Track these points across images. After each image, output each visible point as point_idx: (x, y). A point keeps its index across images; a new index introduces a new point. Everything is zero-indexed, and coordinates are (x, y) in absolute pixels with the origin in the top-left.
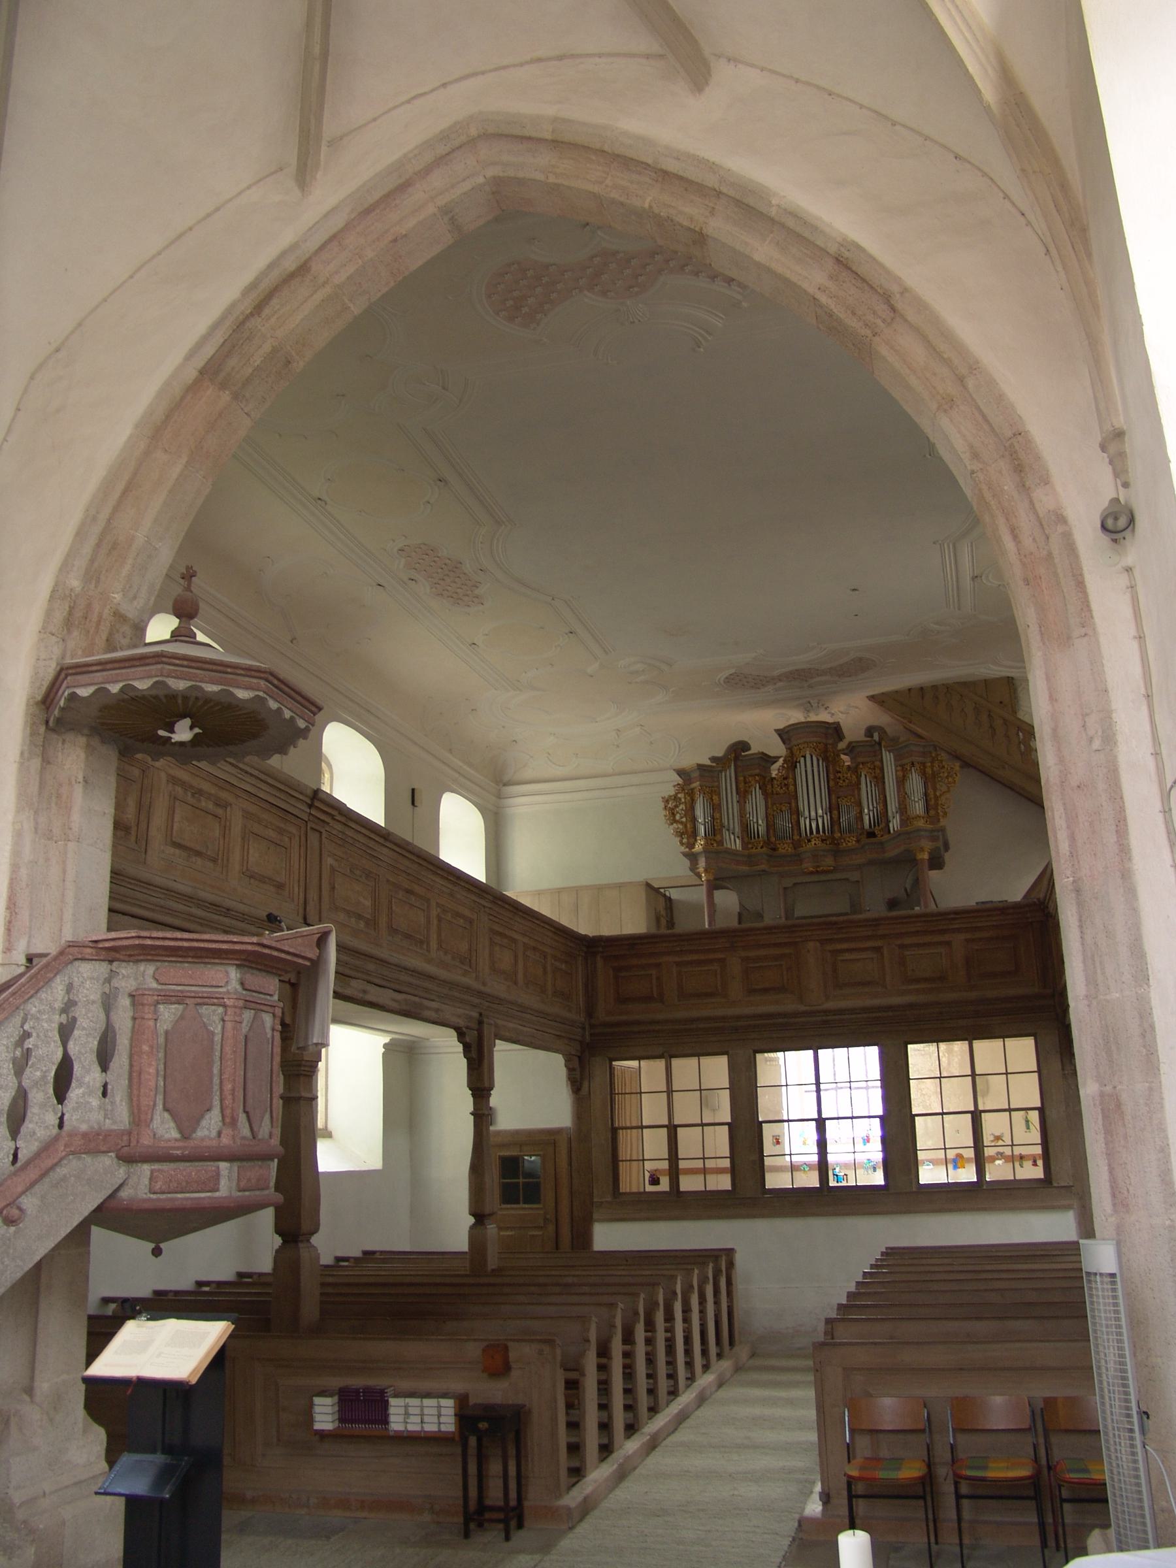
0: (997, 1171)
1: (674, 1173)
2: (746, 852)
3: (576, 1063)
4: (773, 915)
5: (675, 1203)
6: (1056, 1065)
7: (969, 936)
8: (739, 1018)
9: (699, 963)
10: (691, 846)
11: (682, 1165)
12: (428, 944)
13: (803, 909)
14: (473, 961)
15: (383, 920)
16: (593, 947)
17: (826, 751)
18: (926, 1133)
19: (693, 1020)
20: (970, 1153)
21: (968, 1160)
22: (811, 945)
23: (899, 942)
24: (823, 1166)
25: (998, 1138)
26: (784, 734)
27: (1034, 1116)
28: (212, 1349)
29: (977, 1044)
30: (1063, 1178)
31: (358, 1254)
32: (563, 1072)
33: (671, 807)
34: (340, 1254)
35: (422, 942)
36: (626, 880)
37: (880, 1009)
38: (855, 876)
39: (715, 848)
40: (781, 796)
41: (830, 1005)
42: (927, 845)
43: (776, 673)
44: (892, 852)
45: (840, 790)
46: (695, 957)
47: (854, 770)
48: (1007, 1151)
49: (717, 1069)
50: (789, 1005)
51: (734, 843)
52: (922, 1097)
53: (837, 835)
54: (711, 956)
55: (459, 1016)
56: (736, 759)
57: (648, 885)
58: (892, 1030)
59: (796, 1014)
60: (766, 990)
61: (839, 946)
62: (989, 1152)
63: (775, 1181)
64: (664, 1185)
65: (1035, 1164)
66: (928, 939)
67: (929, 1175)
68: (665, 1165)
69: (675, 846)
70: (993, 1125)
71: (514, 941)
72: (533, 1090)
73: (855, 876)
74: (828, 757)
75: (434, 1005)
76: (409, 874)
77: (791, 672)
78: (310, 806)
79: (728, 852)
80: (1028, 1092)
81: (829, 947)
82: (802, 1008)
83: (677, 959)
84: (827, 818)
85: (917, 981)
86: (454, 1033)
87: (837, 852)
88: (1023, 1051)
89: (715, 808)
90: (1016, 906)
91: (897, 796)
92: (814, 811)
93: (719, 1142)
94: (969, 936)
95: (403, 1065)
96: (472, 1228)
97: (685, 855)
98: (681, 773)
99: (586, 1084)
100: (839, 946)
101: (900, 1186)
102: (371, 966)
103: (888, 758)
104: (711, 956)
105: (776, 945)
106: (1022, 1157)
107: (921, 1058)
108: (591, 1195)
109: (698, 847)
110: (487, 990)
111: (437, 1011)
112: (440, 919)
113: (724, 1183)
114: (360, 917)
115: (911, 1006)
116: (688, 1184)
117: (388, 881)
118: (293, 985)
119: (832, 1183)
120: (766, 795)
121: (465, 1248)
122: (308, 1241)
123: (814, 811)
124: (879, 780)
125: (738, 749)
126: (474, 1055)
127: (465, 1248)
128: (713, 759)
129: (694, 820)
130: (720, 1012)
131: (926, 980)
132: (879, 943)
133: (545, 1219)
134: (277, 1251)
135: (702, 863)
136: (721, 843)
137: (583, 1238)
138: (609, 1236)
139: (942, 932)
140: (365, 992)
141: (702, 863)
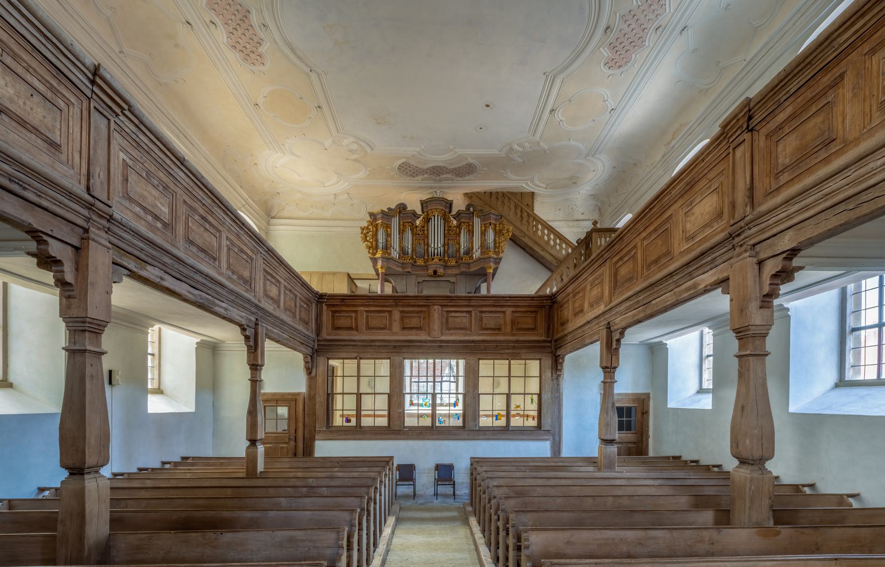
0: (516, 422)
1: (359, 416)
2: (401, 261)
3: (309, 359)
4: (412, 291)
5: (358, 432)
6: (548, 374)
7: (514, 309)
8: (398, 341)
9: (379, 312)
10: (374, 254)
11: (363, 413)
12: (220, 262)
13: (426, 292)
14: (253, 285)
15: (180, 230)
16: (321, 298)
17: (445, 215)
18: (485, 403)
19: (373, 341)
20: (504, 413)
21: (503, 416)
22: (436, 307)
23: (480, 309)
24: (433, 416)
25: (518, 407)
26: (423, 204)
27: (535, 398)
28: (767, 85)
29: (512, 361)
30: (546, 425)
31: (178, 460)
32: (302, 364)
33: (365, 232)
34: (165, 460)
35: (215, 259)
36: (339, 271)
37: (468, 342)
38: (453, 279)
39: (387, 259)
40: (421, 235)
41: (443, 338)
42: (493, 265)
43: (426, 167)
44: (473, 269)
45: (451, 235)
46: (376, 309)
47: (459, 226)
48: (522, 413)
49: (384, 366)
50: (423, 336)
51: (395, 254)
52: (484, 385)
53: (446, 258)
54: (384, 309)
55: (242, 317)
56: (400, 212)
57: (348, 275)
58: (473, 351)
59: (426, 341)
60: (411, 328)
61: (450, 309)
62: (513, 413)
63: (409, 422)
64: (353, 422)
65: (533, 419)
66: (494, 309)
67: (484, 422)
68: (355, 413)
69: (366, 255)
70: (516, 400)
71: (278, 281)
72: (285, 371)
73: (453, 279)
74: (446, 219)
75: (223, 305)
76: (204, 205)
77: (434, 168)
78: (93, 82)
79: (392, 259)
80: (534, 386)
81: (445, 309)
82: (429, 338)
83: (367, 309)
84: (442, 249)
85: (487, 329)
86: (238, 329)
87: (446, 267)
88: (534, 366)
89: (388, 235)
90: (531, 298)
91: (476, 240)
92: (436, 242)
93: (382, 403)
94: (514, 309)
95: (209, 352)
96: (248, 448)
97: (371, 259)
98: (371, 214)
99: (314, 370)
100: (450, 309)
101: (469, 428)
102: (167, 260)
103: (477, 222)
104: (384, 309)
105: (418, 306)
106: (528, 416)
107: (485, 367)
108: (315, 427)
109: (378, 255)
110: (261, 305)
111: (226, 309)
112: (229, 249)
113: (383, 422)
114: (157, 218)
115: (483, 341)
116: (366, 422)
117: (185, 202)
118: (77, 249)
119: (438, 424)
120: (412, 233)
121: (244, 456)
122: (97, 472)
123: (436, 242)
124: (471, 232)
125: (402, 208)
126: (252, 343)
127: (244, 456)
128: (389, 209)
129: (377, 241)
130: (387, 338)
131: (492, 329)
132: (470, 309)
133: (290, 439)
134: (108, 461)
135: (380, 264)
136: (389, 254)
137: (308, 450)
138: (324, 448)
139: (502, 306)
140: (162, 278)
141: (380, 264)
